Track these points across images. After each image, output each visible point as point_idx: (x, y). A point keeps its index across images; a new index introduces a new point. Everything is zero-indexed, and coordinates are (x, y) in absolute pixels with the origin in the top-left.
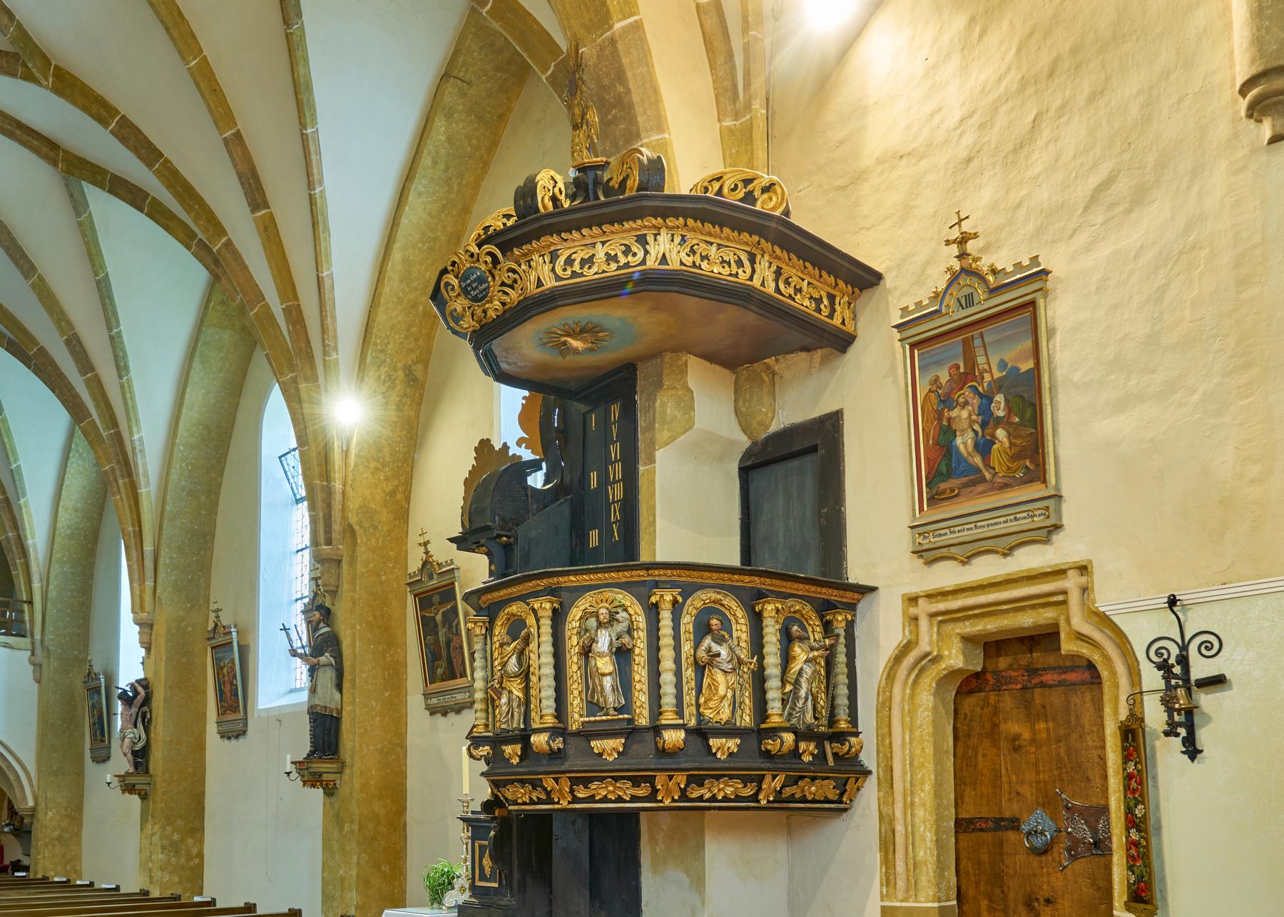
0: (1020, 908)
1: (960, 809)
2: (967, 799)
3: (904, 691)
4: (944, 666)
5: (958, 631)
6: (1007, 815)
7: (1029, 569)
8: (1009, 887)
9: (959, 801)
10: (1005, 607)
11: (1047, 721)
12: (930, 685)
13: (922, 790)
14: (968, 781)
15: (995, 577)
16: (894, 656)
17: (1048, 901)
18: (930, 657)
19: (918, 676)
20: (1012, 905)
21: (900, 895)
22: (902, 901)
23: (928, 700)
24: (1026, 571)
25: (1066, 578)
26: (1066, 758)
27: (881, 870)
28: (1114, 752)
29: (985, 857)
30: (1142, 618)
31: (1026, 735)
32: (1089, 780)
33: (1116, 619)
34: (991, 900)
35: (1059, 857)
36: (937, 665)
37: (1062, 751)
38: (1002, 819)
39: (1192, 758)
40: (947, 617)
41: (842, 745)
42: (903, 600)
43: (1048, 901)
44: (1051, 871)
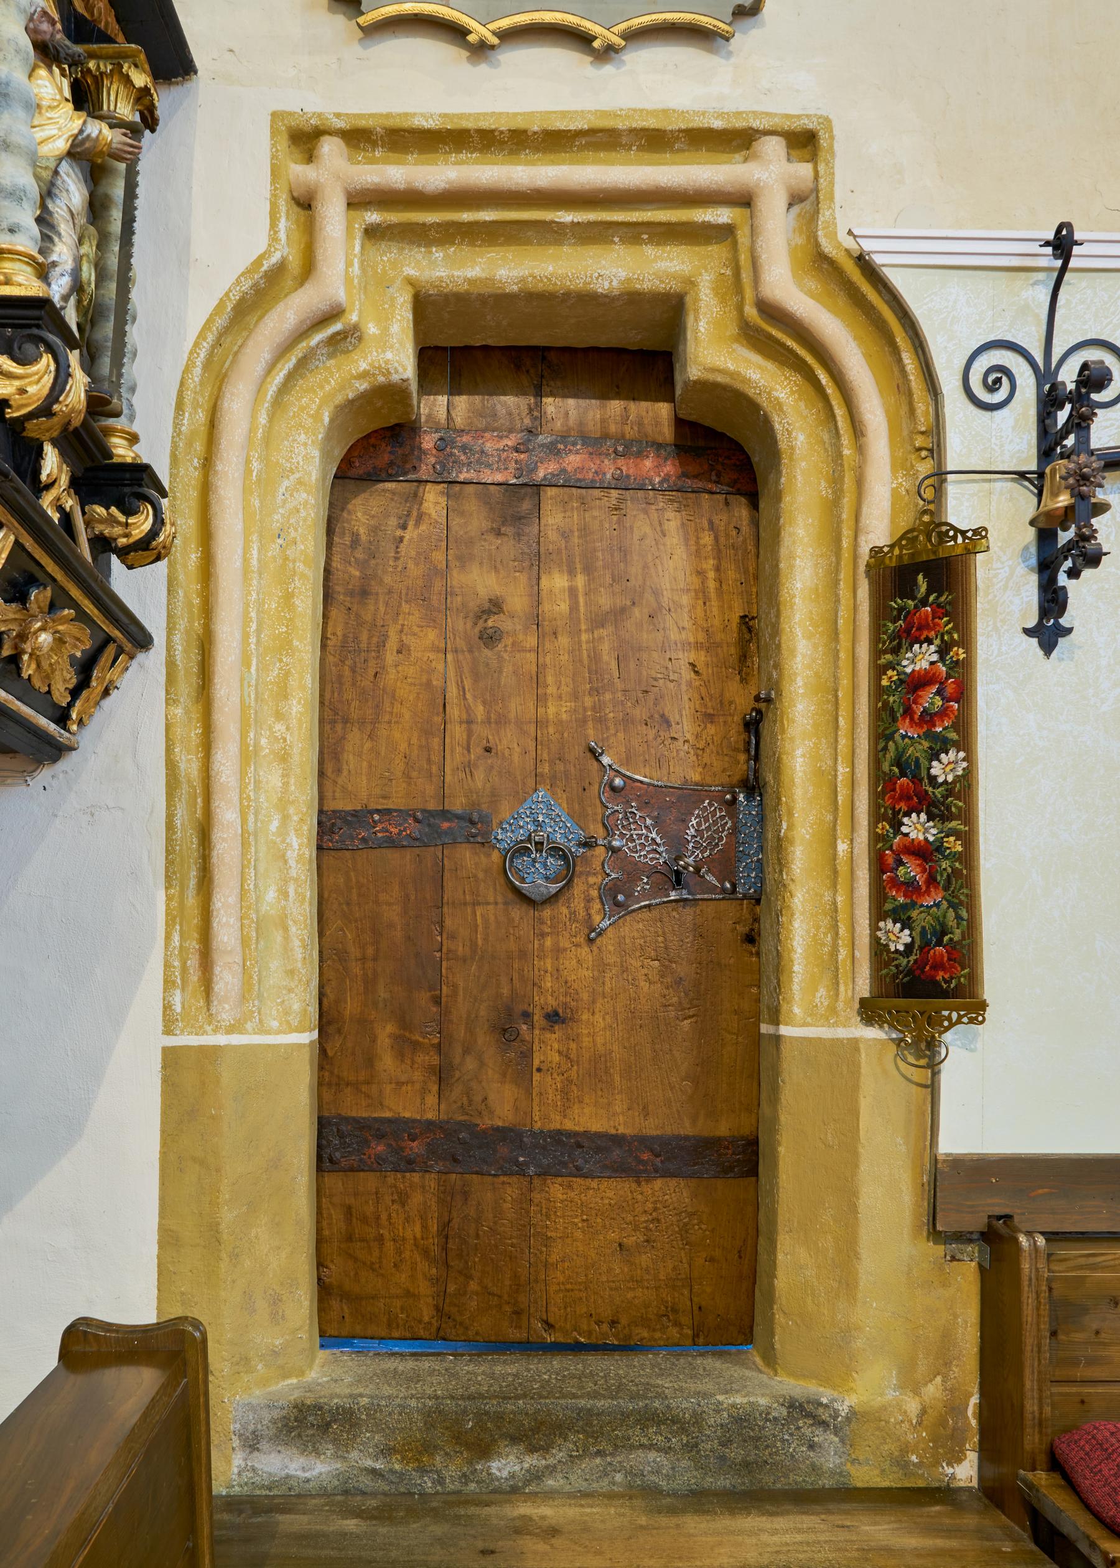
0: (480, 1041)
1: (328, 784)
2: (350, 760)
3: (254, 416)
4: (363, 366)
5: (411, 271)
6: (457, 805)
7: (665, 111)
8: (455, 986)
9: (329, 769)
10: (566, 217)
11: (572, 572)
12: (317, 417)
13: (279, 716)
14: (354, 715)
15: (564, 114)
16: (235, 297)
17: (554, 1018)
18: (337, 327)
19: (290, 377)
20: (461, 1033)
21: (226, 1012)
22: (231, 1030)
23: (306, 457)
24: (653, 113)
25: (755, 157)
26: (614, 665)
27: (168, 937)
28: (809, 636)
29: (392, 914)
30: (956, 287)
31: (517, 601)
32: (668, 723)
33: (896, 278)
34: (404, 1023)
35: (587, 909)
36: (341, 358)
37: (605, 647)
38: (445, 814)
39: (1048, 647)
40: (394, 217)
41: (129, 512)
42: (274, 132)
43: (554, 1018)
44: (564, 943)
